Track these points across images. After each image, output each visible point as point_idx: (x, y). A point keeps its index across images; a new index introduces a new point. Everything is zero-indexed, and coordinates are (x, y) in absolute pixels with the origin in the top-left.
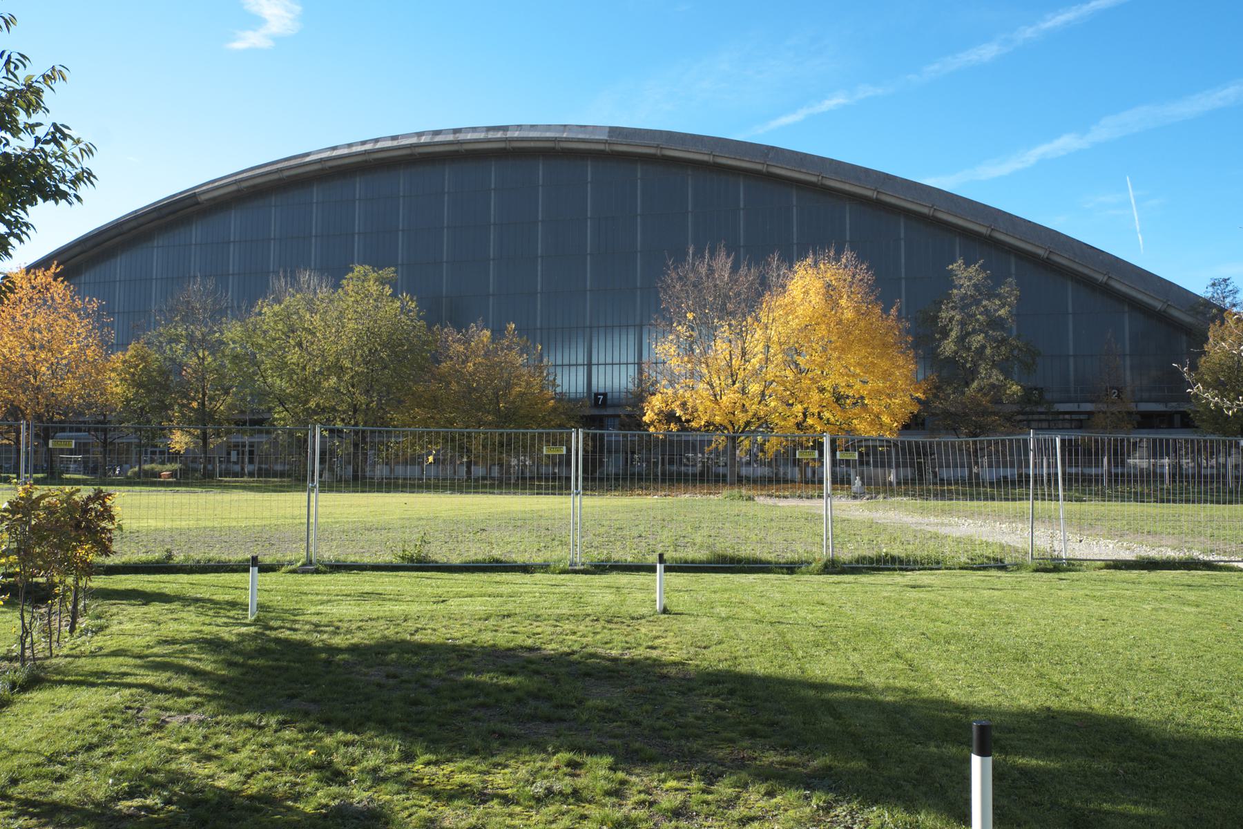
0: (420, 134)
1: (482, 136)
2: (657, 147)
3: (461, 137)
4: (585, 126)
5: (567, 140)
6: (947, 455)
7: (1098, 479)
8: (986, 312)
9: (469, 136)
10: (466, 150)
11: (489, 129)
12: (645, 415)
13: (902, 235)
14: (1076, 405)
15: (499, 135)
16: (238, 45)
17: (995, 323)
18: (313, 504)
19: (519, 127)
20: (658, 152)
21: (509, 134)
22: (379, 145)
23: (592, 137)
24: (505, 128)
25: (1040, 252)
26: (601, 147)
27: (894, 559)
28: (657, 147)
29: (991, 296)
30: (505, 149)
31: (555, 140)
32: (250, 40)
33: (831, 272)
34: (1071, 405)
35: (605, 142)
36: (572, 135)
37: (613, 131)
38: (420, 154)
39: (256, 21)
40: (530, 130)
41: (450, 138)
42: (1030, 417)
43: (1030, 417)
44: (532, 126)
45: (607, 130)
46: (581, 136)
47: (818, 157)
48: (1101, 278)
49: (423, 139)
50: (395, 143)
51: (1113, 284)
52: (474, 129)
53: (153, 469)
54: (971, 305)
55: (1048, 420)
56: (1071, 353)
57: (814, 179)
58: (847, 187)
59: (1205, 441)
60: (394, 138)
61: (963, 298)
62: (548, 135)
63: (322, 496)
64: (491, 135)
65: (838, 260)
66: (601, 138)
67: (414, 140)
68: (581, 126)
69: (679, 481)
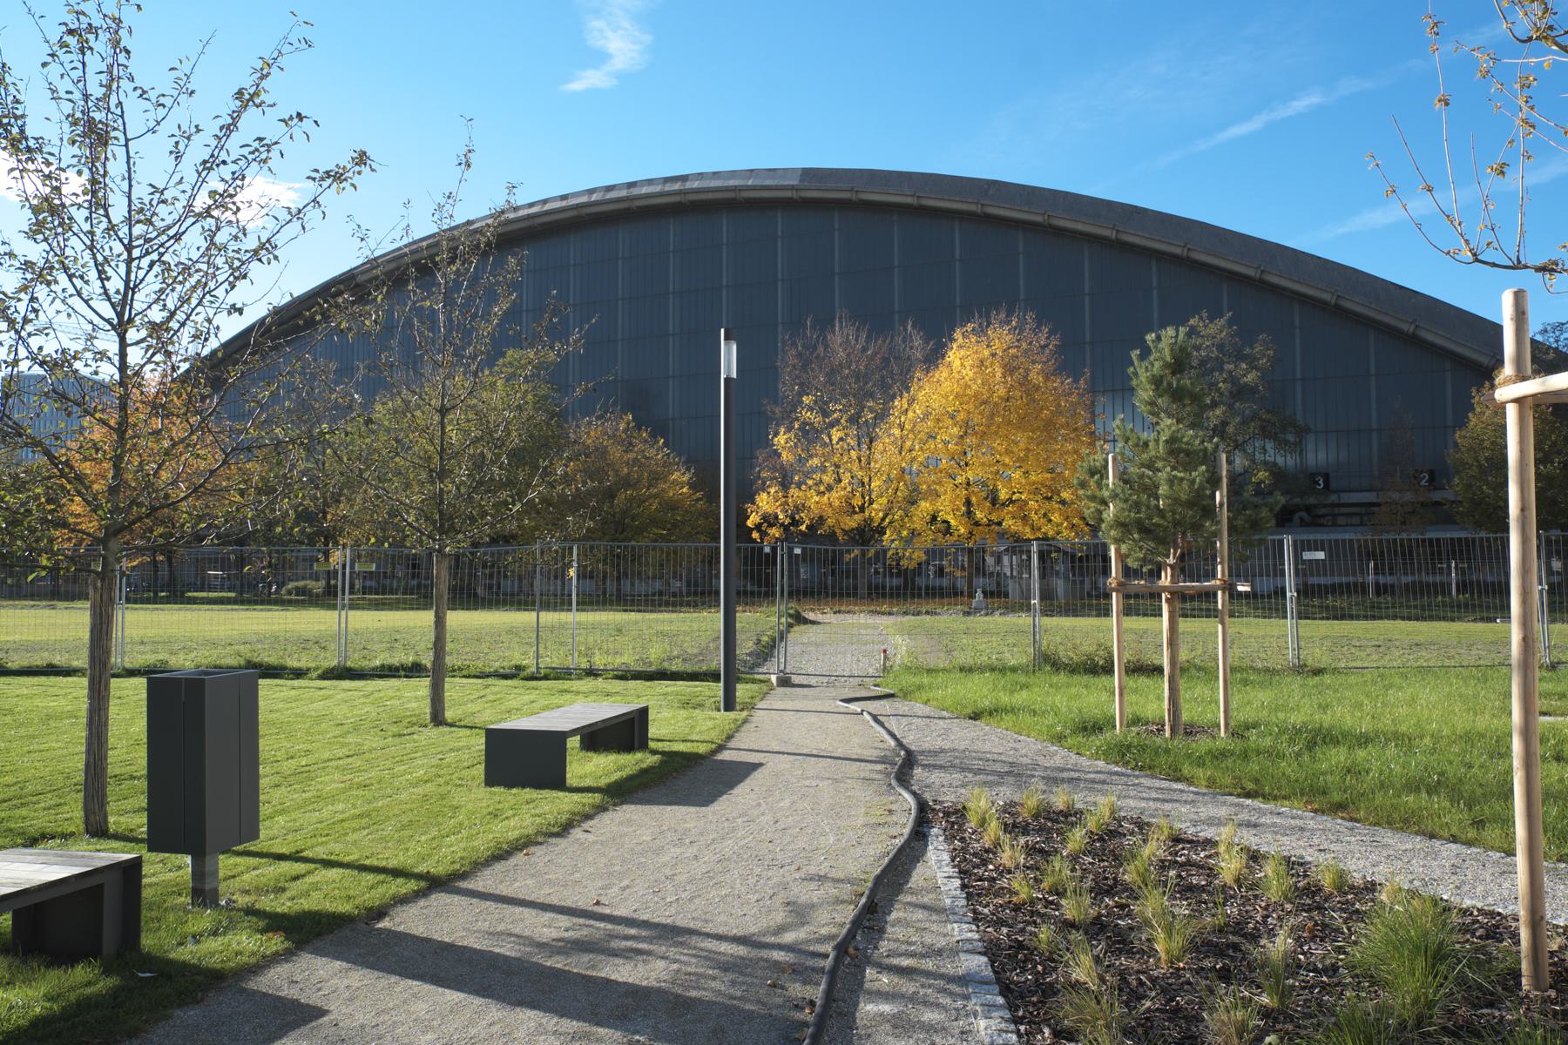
0: (591, 191)
1: (657, 189)
2: (851, 190)
3: (635, 191)
4: (774, 170)
5: (749, 188)
6: (1267, 565)
7: (1362, 589)
8: (1233, 380)
9: (644, 190)
10: (639, 207)
11: (667, 180)
12: (748, 517)
13: (1155, 284)
14: (1374, 494)
15: (677, 186)
16: (576, 86)
17: (1241, 392)
18: (343, 620)
19: (701, 176)
20: (854, 197)
21: (689, 185)
22: (548, 207)
23: (781, 183)
24: (684, 178)
25: (1326, 297)
26: (788, 194)
27: (381, 677)
28: (851, 190)
29: (1240, 357)
30: (680, 203)
31: (735, 189)
32: (591, 79)
33: (1001, 337)
34: (1368, 494)
35: (792, 188)
36: (758, 182)
37: (808, 173)
38: (589, 215)
39: (599, 58)
40: (711, 179)
41: (623, 193)
42: (1336, 510)
43: (1336, 510)
44: (714, 173)
45: (800, 172)
46: (768, 182)
47: (1050, 190)
48: (1407, 327)
49: (594, 197)
50: (564, 204)
51: (1423, 334)
52: (650, 182)
53: (305, 586)
54: (1212, 370)
55: (1360, 514)
56: (1375, 427)
57: (1039, 219)
58: (1080, 227)
59: (1373, 541)
60: (564, 197)
61: (1203, 363)
62: (732, 183)
63: (351, 613)
64: (669, 187)
65: (1008, 323)
66: (791, 183)
67: (584, 199)
68: (770, 170)
69: (934, 596)
